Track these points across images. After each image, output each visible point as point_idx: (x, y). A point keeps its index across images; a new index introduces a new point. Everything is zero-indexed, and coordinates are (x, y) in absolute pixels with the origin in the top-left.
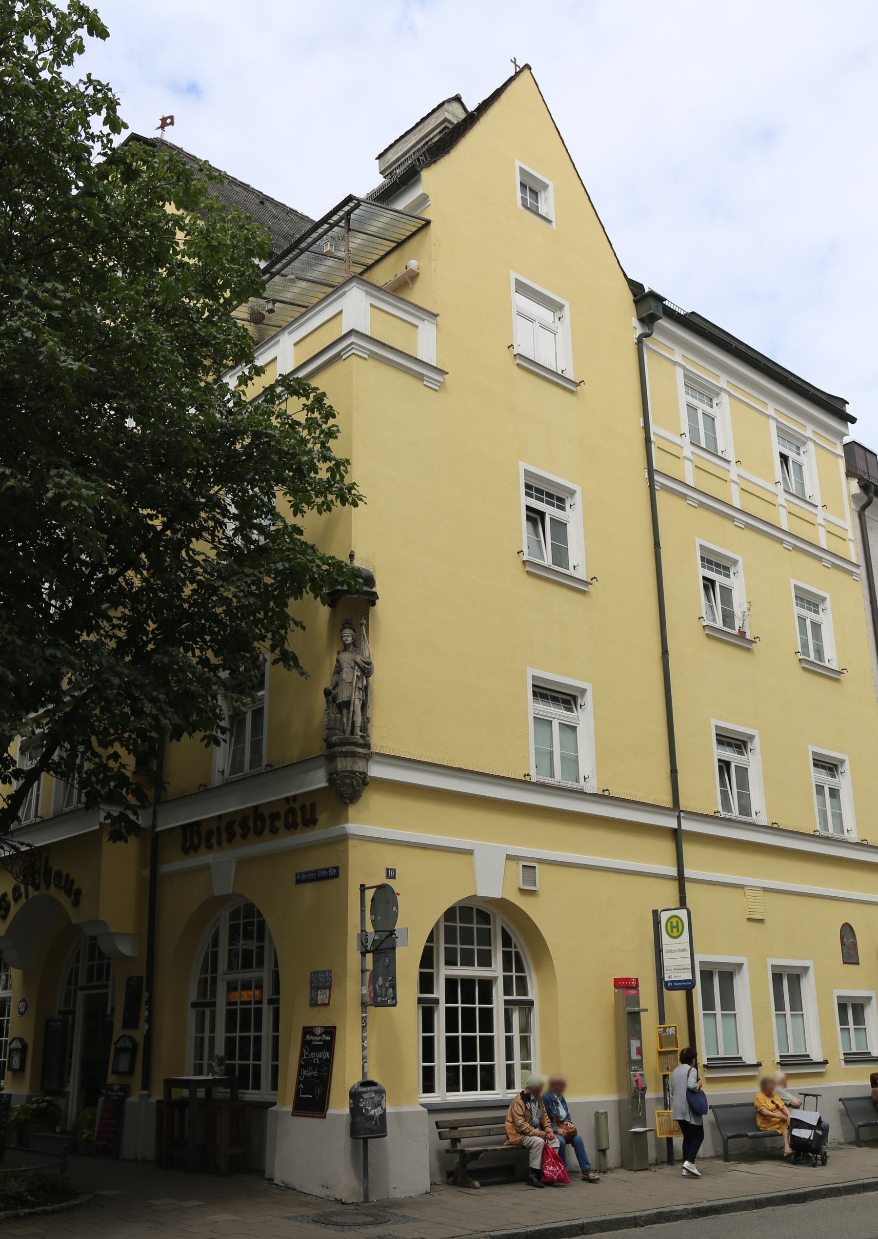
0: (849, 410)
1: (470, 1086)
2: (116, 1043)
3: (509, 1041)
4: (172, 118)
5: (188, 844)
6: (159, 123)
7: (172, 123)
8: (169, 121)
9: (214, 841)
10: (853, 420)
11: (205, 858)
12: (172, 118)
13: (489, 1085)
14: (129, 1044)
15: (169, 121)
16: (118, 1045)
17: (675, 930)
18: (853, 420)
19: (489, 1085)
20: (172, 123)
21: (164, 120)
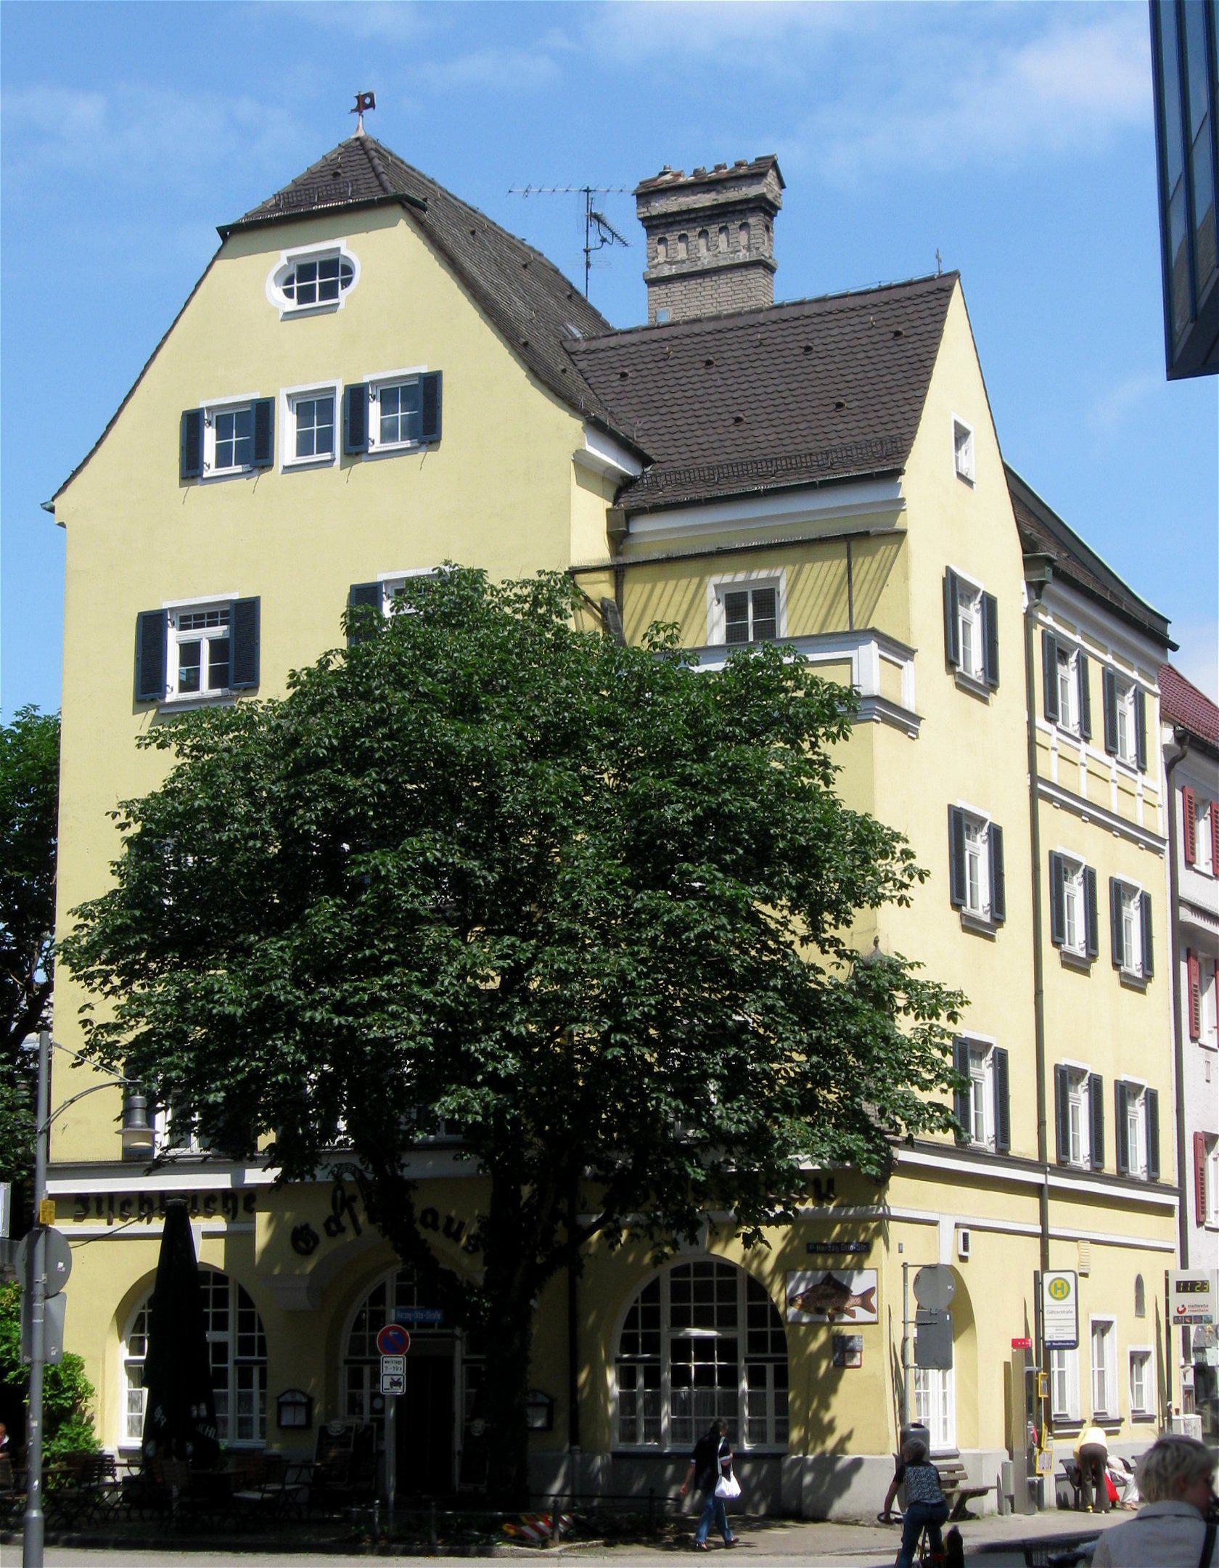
0: (1173, 634)
4: (371, 95)
6: (355, 104)
7: (372, 105)
8: (368, 101)
10: (1175, 647)
12: (371, 95)
15: (368, 101)
17: (1060, 1290)
18: (1175, 647)
20: (372, 105)
21: (360, 98)
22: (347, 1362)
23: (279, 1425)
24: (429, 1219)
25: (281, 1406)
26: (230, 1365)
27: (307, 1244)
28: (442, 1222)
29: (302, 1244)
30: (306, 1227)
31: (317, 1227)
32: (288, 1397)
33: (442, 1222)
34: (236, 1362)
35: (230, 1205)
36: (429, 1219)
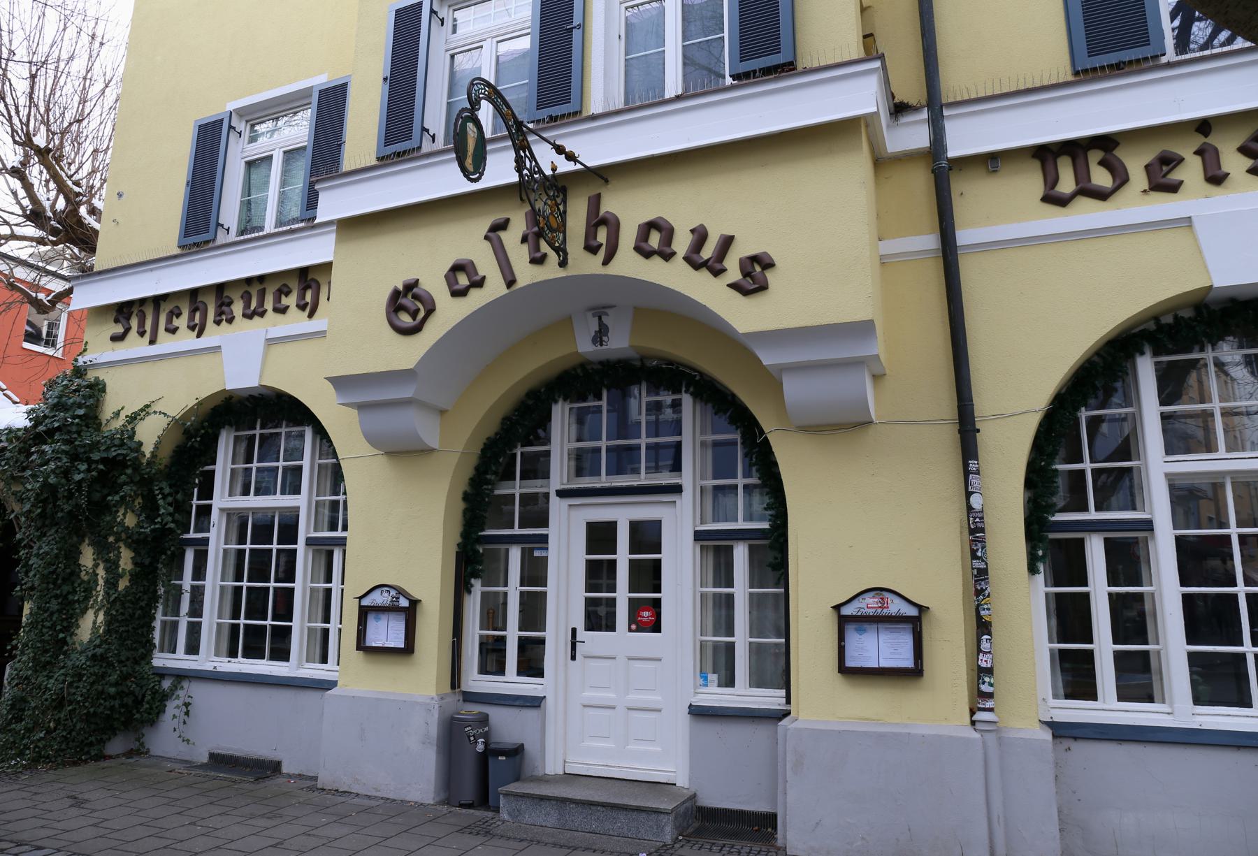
1: (253, 651)
2: (360, 598)
3: (196, 610)
5: (1067, 184)
9: (1191, 171)
11: (1136, 206)
13: (281, 654)
14: (896, 607)
16: (365, 602)
19: (281, 654)
22: (152, 342)
23: (361, 645)
24: (655, 240)
25: (845, 622)
26: (300, 546)
27: (414, 314)
28: (682, 244)
29: (406, 319)
30: (411, 287)
31: (435, 285)
32: (379, 599)
33: (682, 244)
34: (310, 542)
35: (308, 298)
36: (655, 240)
